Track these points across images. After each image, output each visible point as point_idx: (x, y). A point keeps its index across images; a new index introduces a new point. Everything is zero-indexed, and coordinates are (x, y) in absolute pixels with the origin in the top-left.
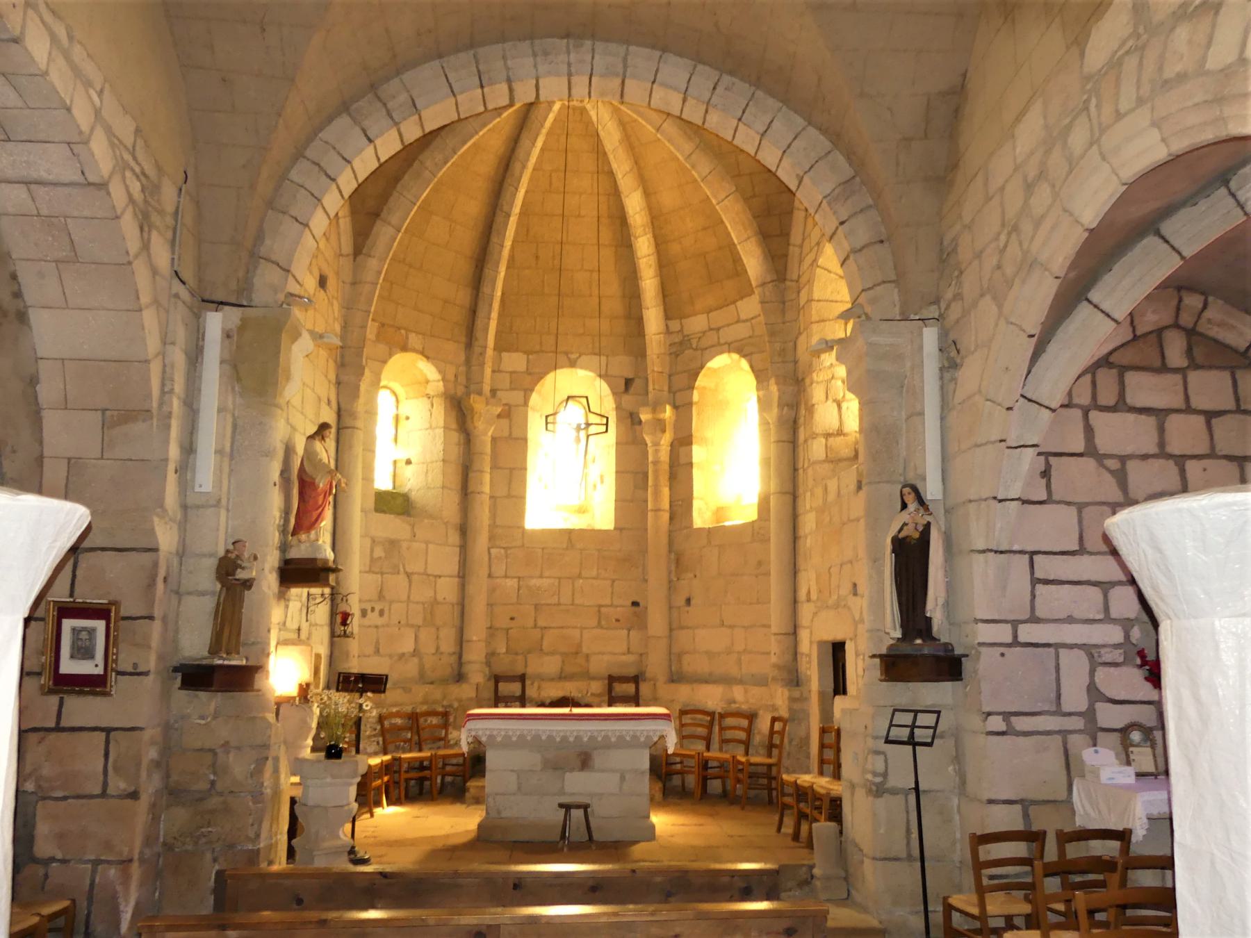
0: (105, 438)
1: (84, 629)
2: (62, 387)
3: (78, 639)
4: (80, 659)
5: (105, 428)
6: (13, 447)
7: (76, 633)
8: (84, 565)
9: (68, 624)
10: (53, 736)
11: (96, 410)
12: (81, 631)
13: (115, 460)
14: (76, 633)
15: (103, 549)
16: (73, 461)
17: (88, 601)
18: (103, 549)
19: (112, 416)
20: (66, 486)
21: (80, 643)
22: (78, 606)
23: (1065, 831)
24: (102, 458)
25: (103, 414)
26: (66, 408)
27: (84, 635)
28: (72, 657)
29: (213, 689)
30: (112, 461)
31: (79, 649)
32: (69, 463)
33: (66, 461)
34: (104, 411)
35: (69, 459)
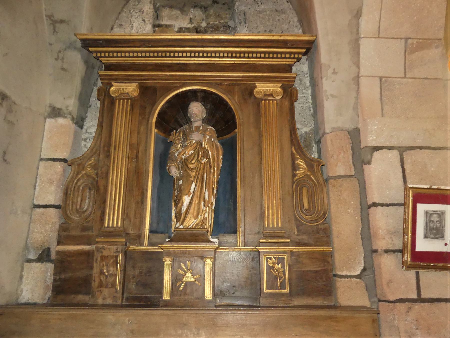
0: (407, 61)
1: (435, 212)
2: (378, 19)
3: (430, 221)
4: (432, 238)
5: (407, 53)
6: (334, 69)
7: (428, 215)
8: (409, 161)
9: (422, 208)
10: (417, 307)
11: (401, 39)
12: (432, 214)
13: (415, 78)
14: (428, 215)
15: (421, 148)
16: (383, 80)
17: (442, 187)
18: (421, 148)
19: (413, 44)
20: (381, 99)
21: (432, 225)
22: (434, 192)
23: (445, 302)
24: (405, 77)
25: (406, 42)
26: (379, 37)
27: (435, 218)
28: (426, 237)
29: (171, 256)
30: (413, 80)
31: (431, 229)
32: (381, 80)
33: (378, 79)
34: (407, 39)
35: (381, 78)
